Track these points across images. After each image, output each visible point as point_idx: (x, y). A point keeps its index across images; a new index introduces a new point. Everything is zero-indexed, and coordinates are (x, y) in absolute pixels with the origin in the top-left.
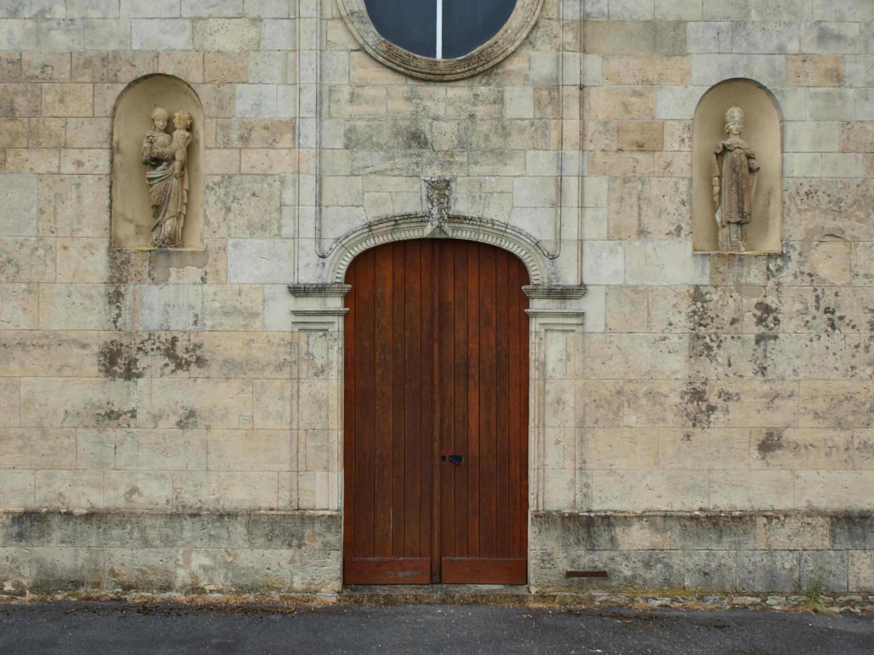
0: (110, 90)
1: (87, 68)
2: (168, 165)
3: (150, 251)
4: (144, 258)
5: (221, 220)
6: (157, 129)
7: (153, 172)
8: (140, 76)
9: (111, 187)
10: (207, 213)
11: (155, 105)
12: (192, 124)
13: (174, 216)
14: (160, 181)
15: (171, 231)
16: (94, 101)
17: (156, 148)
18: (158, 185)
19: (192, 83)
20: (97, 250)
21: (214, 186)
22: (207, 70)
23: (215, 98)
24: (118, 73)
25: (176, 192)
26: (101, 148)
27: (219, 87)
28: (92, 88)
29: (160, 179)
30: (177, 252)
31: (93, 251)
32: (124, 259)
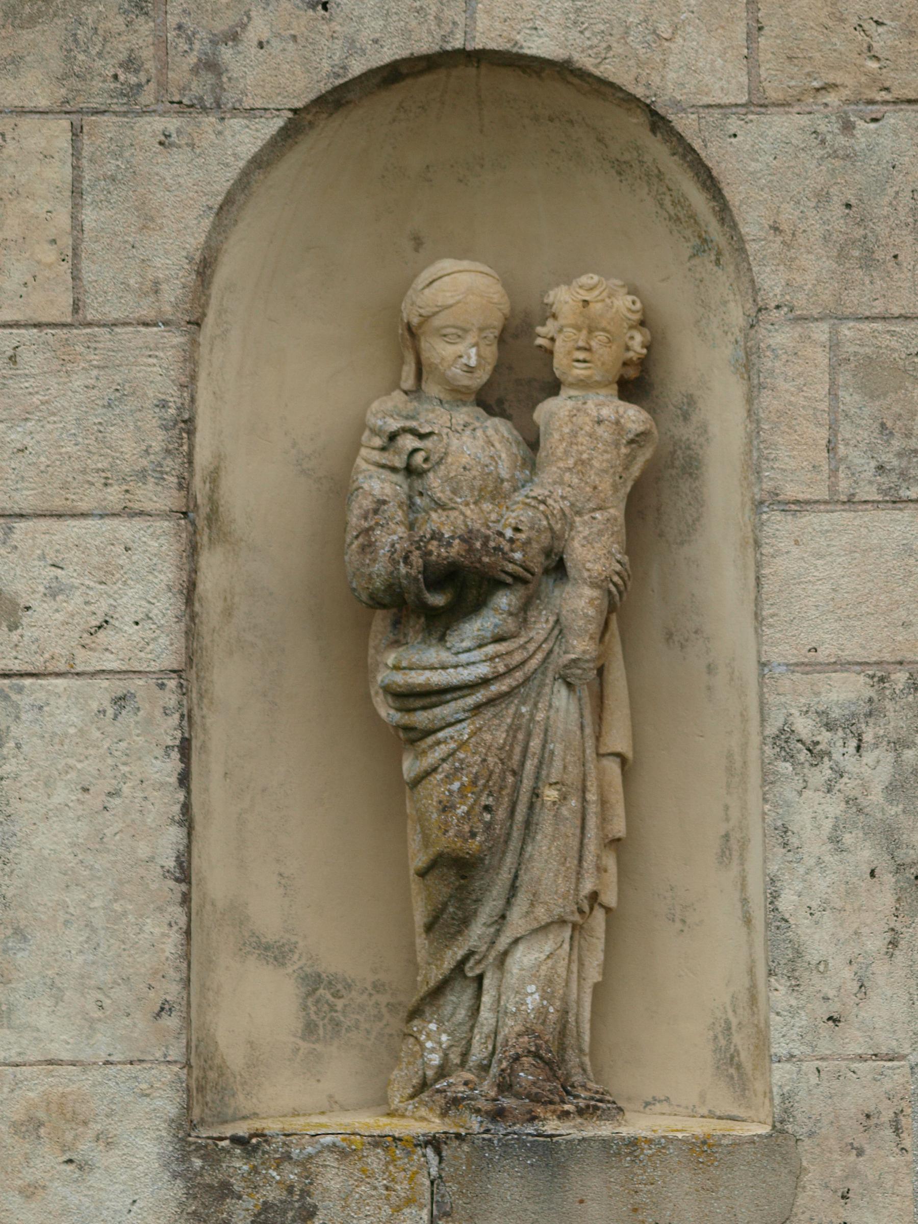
0: (178, 156)
1: (32, 21)
2: (523, 613)
3: (435, 1143)
4: (401, 1188)
5: (876, 943)
6: (431, 388)
7: (434, 654)
8: (357, 68)
9: (185, 748)
10: (787, 902)
11: (418, 242)
12: (644, 364)
13: (562, 922)
14: (477, 708)
15: (542, 1013)
16: (77, 226)
17: (441, 506)
18: (466, 729)
19: (677, 104)
20: (106, 1141)
21: (824, 737)
22: (772, 27)
23: (822, 197)
24: (226, 53)
25: (574, 772)
26: (129, 513)
27: (848, 127)
28: (64, 142)
29: (480, 696)
30: (605, 1143)
31: (85, 1148)
32: (273, 1194)
